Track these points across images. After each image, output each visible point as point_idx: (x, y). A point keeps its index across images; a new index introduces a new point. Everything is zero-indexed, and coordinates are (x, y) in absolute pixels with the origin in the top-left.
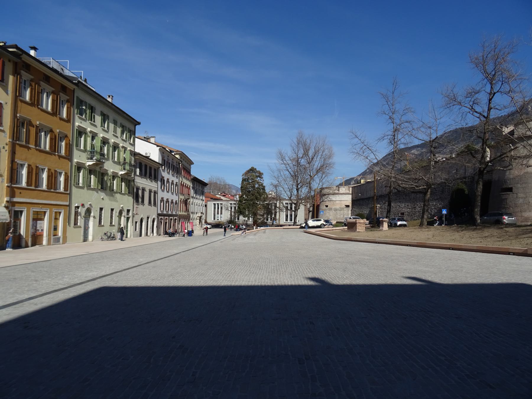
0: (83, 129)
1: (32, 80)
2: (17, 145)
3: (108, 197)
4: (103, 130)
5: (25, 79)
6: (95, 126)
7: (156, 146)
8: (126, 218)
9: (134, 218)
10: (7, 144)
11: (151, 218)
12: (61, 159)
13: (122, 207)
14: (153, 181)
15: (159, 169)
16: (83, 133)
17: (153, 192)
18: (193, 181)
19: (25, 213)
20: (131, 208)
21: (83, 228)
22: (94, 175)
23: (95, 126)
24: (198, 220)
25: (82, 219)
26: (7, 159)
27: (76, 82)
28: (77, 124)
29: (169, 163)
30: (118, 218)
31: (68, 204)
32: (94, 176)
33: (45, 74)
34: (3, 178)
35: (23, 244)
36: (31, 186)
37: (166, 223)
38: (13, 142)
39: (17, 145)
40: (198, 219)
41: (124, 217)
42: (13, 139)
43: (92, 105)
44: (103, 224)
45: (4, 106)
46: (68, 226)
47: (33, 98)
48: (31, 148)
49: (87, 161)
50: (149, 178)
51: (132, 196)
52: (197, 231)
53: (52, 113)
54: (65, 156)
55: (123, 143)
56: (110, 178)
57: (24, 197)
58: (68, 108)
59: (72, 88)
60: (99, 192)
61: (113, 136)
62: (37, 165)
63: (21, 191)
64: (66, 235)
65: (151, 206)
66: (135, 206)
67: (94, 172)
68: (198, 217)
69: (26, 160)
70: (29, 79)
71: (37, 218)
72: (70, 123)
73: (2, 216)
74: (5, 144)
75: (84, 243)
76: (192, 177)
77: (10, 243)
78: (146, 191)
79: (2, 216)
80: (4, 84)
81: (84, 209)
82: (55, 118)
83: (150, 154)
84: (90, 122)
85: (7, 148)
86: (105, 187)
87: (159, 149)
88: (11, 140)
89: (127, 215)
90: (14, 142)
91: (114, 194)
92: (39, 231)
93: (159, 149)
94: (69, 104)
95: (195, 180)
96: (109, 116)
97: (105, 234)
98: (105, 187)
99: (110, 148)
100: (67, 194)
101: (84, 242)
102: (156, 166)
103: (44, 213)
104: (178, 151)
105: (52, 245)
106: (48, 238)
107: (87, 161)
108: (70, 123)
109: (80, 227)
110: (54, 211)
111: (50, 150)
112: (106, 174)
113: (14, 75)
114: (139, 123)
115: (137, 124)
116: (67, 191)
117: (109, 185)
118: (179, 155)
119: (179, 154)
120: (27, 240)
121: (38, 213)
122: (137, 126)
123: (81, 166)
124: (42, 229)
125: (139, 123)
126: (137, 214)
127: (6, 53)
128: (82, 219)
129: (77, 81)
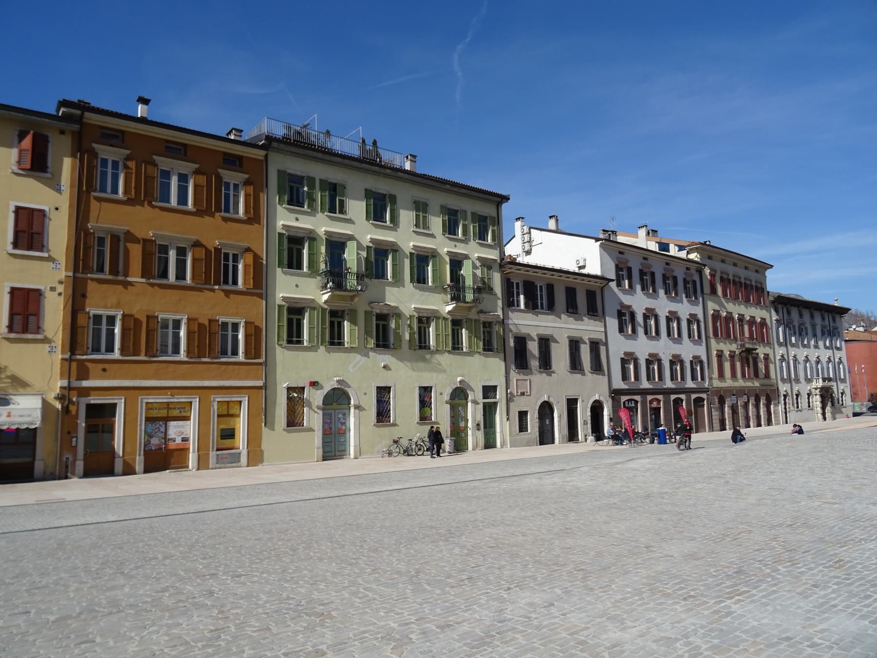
0: (302, 231)
1: (128, 158)
2: (89, 281)
3: (409, 364)
4: (331, 220)
5: (114, 159)
6: (432, 236)
7: (594, 241)
8: (481, 407)
9: (511, 404)
10: (61, 282)
11: (583, 401)
12: (232, 296)
13: (460, 382)
14: (563, 316)
15: (606, 292)
16: (430, 257)
17: (587, 341)
18: (780, 307)
19: (245, 403)
20: (498, 380)
21: (321, 432)
22: (348, 321)
23: (432, 236)
24: (818, 397)
25: (316, 412)
26: (62, 309)
27: (263, 142)
28: (280, 223)
29: (675, 279)
30: (448, 406)
31: (262, 385)
32: (349, 323)
33: (225, 154)
34: (53, 344)
35: (119, 466)
36: (139, 355)
37: (658, 410)
38: (74, 277)
39: (89, 281)
40: (816, 395)
41: (475, 402)
42: (76, 270)
43: (334, 181)
44: (395, 420)
45: (53, 215)
46: (265, 430)
47: (252, 210)
48: (134, 283)
49: (321, 293)
50: (568, 312)
51: (502, 355)
52: (817, 422)
53: (195, 210)
54: (245, 290)
55: (455, 246)
56: (409, 323)
57: (114, 378)
58: (247, 196)
59: (261, 156)
60: (371, 354)
61: (413, 233)
62: (155, 313)
63: (106, 366)
64: (260, 446)
65: (584, 374)
66: (514, 375)
67: (466, 322)
68: (816, 389)
69: (118, 306)
70: (123, 157)
71: (168, 417)
72: (259, 224)
73: (21, 416)
74: (57, 282)
75: (324, 462)
76: (771, 298)
77: (80, 465)
78: (557, 342)
79: (21, 416)
80: (48, 175)
81: (319, 392)
82: (207, 219)
83: (585, 260)
84: (371, 223)
85: (60, 288)
86: (496, 347)
87: (600, 246)
88: (71, 274)
89: (483, 398)
90: (79, 275)
91: (428, 356)
92: (175, 441)
93: (601, 246)
94: (252, 187)
95: (783, 303)
96: (395, 196)
97: (396, 442)
98: (496, 347)
99: (405, 260)
100: (260, 364)
101: (323, 460)
102: (595, 285)
103: (239, 404)
104: (693, 244)
105: (212, 469)
106: (199, 456)
107: (321, 293)
108: (259, 224)
109: (311, 430)
110: (214, 401)
111: (193, 282)
112: (393, 316)
113: (73, 156)
114: (506, 198)
115: (499, 199)
116: (258, 356)
117: (407, 337)
118: (698, 253)
119: (697, 250)
120: (130, 462)
121: (170, 406)
122: (504, 206)
123: (303, 306)
124: (182, 436)
125: (506, 198)
126: (523, 394)
127: (39, 119)
128: (316, 412)
129: (265, 140)
